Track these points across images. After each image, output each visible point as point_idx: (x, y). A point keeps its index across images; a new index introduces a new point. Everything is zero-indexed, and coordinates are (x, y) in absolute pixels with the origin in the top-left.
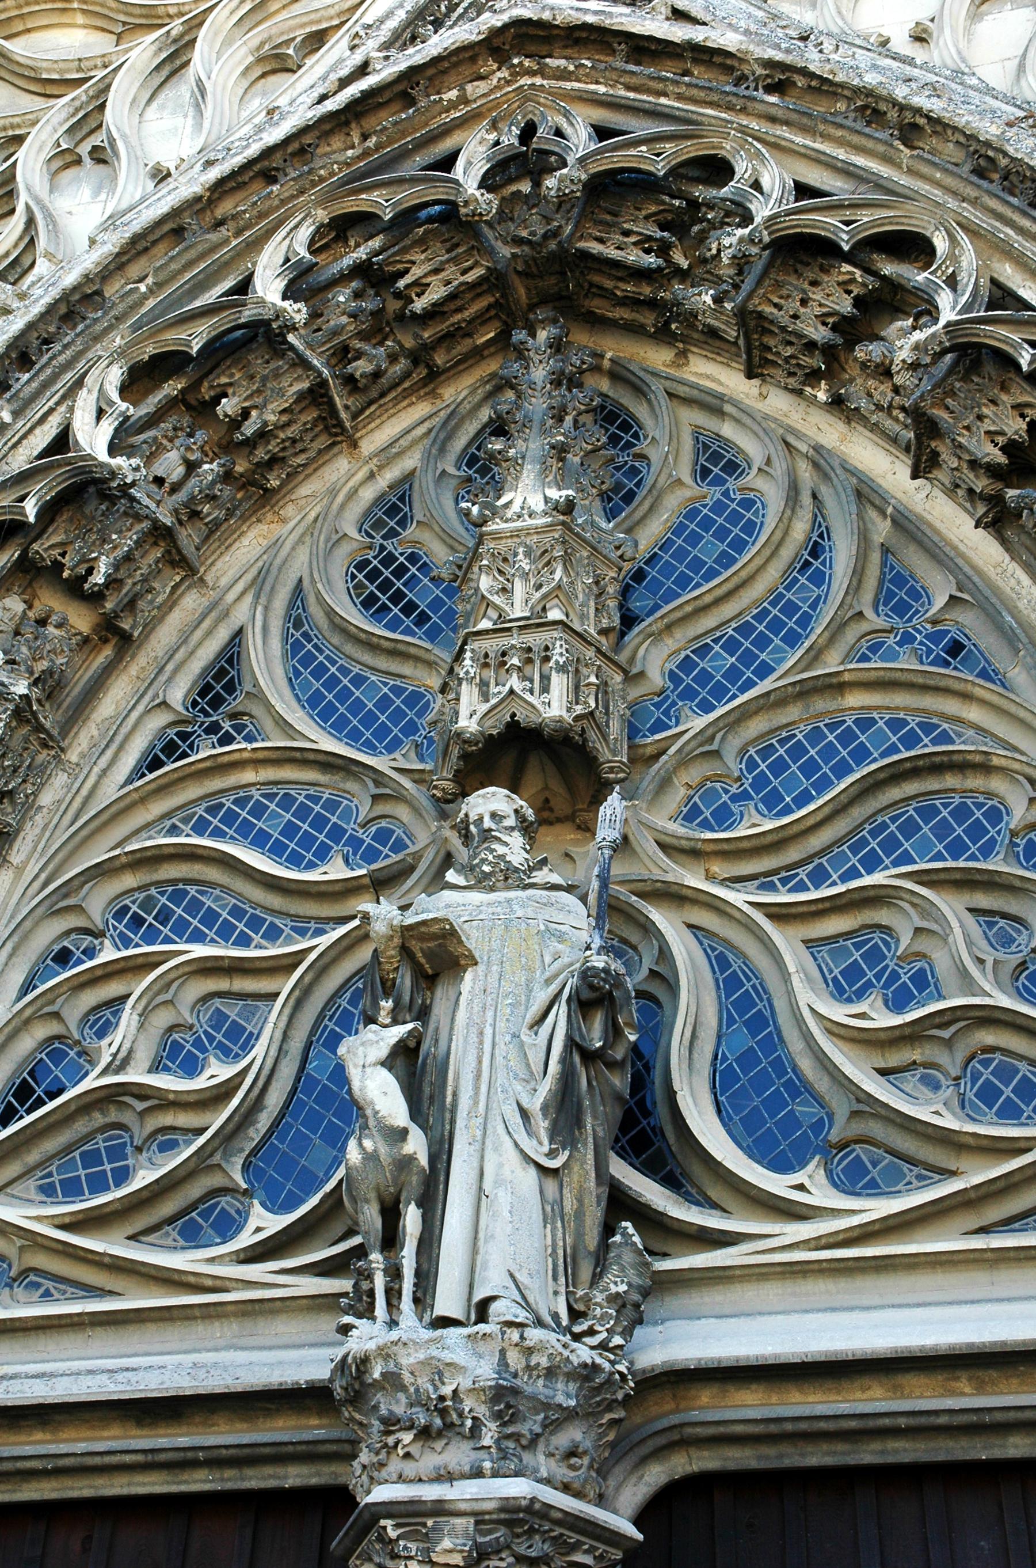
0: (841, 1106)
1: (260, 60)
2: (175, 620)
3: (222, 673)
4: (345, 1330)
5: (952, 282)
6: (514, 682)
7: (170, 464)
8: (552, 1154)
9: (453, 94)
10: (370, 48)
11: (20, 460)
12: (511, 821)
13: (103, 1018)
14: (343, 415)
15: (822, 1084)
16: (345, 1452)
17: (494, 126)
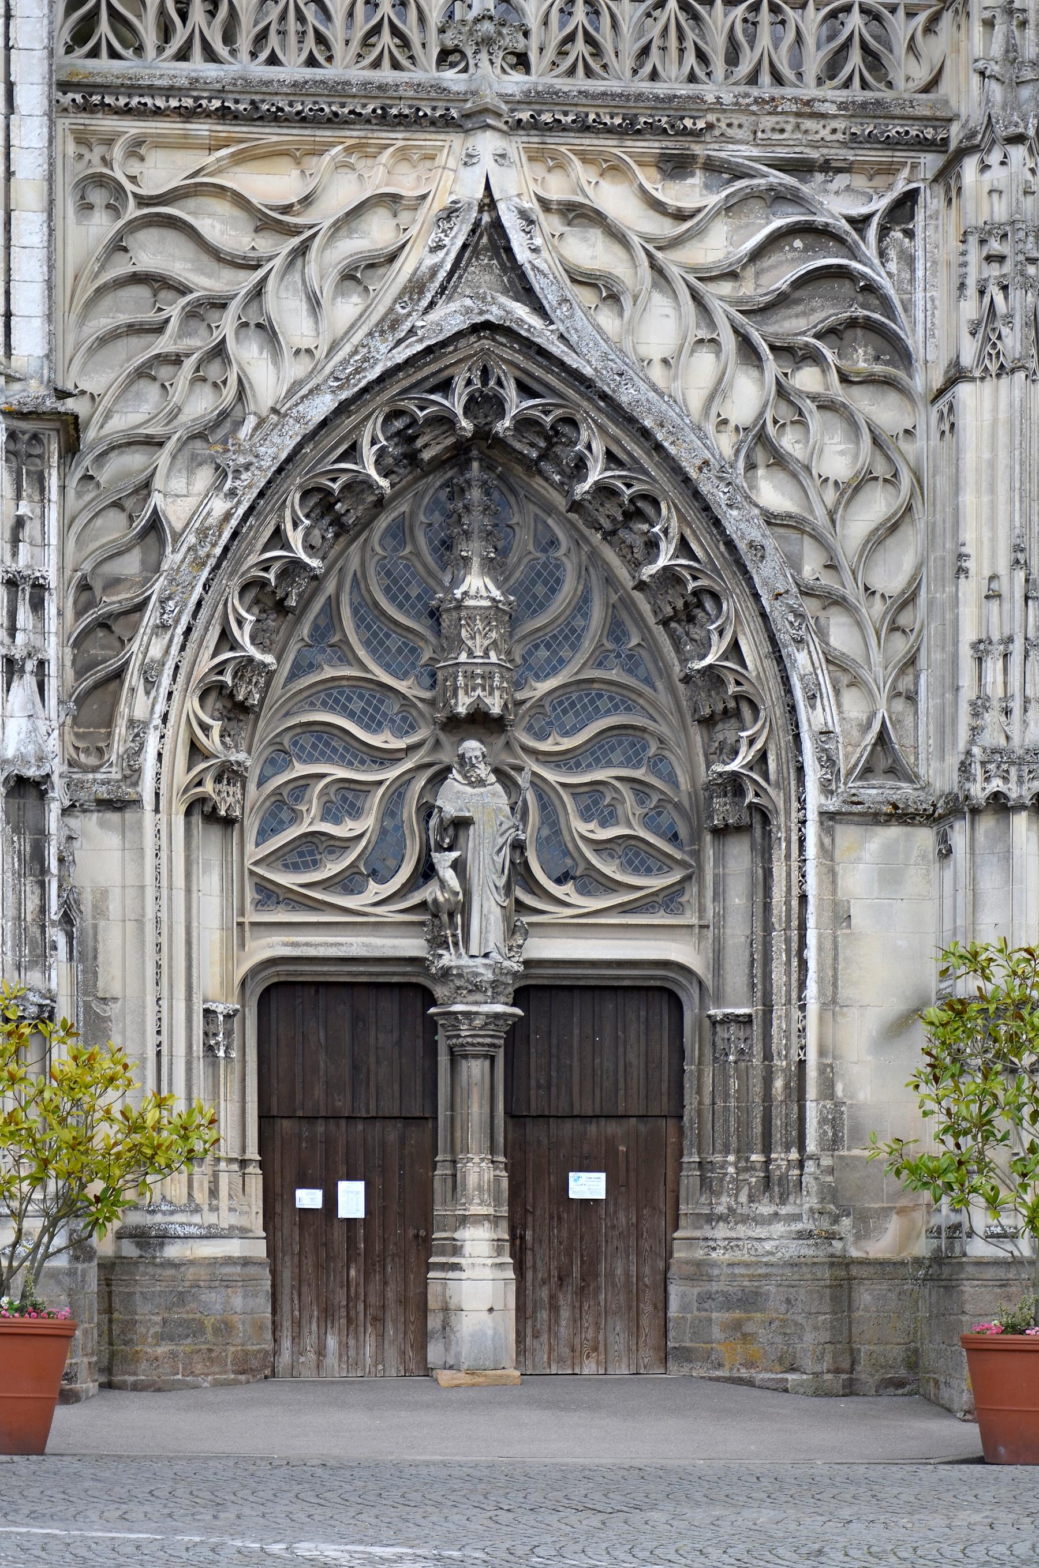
15: (576, 855)
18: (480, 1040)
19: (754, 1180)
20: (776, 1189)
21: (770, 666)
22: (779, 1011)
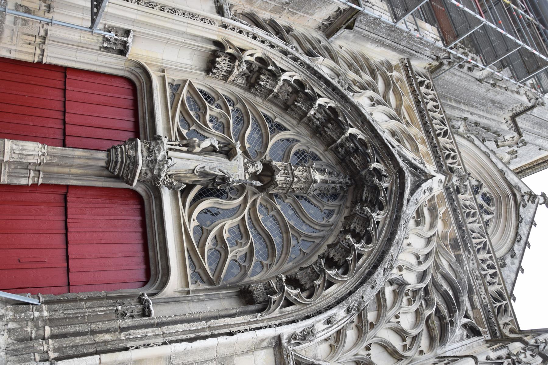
0: (209, 228)
1: (394, 132)
2: (291, 120)
3: (282, 128)
4: (166, 137)
5: (363, 247)
6: (282, 171)
7: (319, 116)
8: (197, 172)
9: (391, 163)
10: (397, 148)
11: (316, 90)
12: (257, 170)
13: (218, 106)
14: (331, 147)
15: (212, 225)
16: (146, 138)
17: (385, 170)
18: (120, 155)
19: (29, 329)
20: (21, 346)
21: (331, 300)
22: (158, 331)
